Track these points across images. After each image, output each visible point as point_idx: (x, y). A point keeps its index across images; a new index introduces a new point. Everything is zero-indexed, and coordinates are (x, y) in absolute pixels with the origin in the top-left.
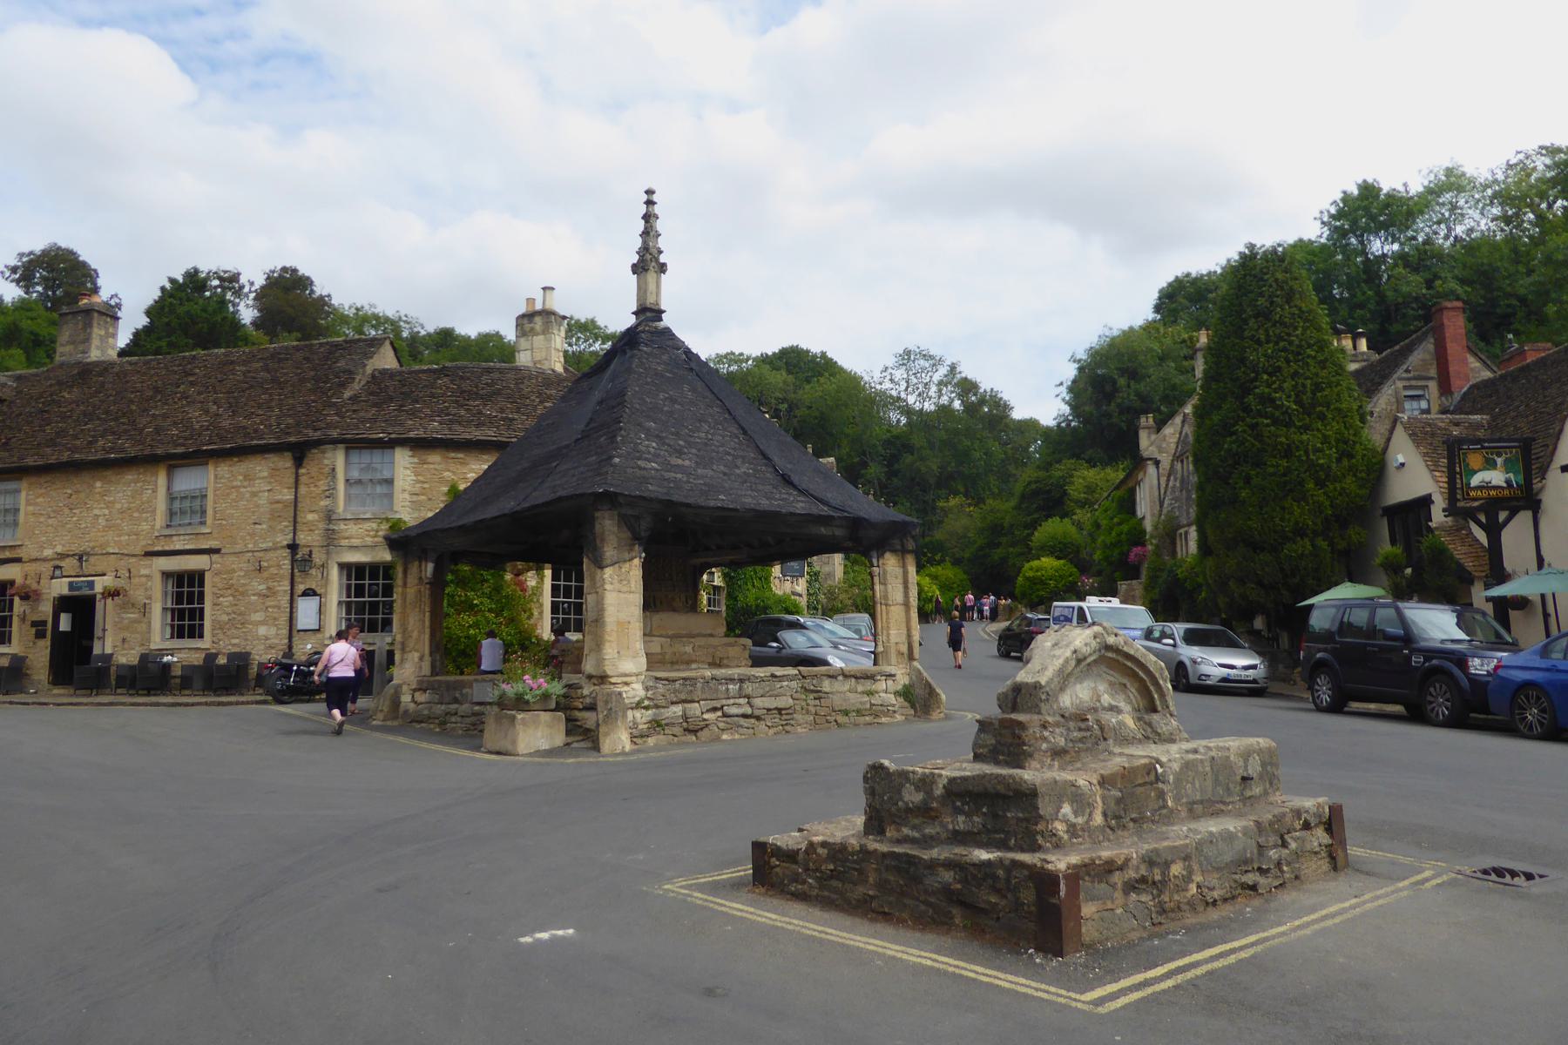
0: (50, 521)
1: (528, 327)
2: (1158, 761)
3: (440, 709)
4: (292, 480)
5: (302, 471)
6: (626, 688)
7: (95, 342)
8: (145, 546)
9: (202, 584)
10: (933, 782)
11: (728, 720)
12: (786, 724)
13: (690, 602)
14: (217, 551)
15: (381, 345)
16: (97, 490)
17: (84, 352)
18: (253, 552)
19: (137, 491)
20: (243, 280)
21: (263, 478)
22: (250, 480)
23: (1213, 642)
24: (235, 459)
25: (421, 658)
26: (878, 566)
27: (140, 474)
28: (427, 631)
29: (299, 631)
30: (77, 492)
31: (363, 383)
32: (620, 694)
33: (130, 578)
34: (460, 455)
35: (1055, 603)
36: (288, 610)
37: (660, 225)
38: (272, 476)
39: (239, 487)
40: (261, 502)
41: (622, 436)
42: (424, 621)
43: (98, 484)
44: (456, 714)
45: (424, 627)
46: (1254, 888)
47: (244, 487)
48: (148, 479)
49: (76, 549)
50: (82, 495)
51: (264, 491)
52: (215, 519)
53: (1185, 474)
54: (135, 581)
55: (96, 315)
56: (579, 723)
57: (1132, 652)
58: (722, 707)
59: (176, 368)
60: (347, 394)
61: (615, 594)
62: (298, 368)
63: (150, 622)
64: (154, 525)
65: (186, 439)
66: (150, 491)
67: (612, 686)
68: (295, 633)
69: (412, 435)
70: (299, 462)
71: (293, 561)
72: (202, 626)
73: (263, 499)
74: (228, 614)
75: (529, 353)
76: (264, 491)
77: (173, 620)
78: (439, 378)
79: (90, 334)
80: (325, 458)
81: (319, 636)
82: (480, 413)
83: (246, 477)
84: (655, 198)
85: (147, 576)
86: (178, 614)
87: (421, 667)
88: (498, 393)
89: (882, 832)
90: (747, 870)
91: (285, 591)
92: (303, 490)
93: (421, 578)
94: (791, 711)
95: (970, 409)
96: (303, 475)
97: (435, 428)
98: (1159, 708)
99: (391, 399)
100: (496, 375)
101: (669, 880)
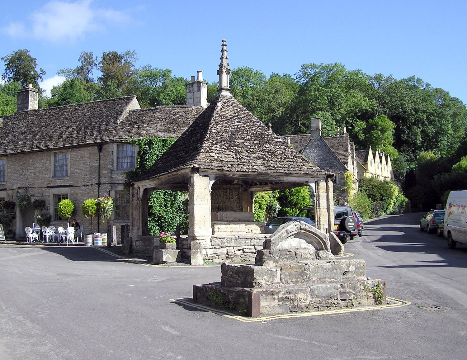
4: (98, 158)
7: (30, 103)
8: (47, 184)
11: (245, 254)
14: (72, 186)
16: (31, 163)
23: (376, 224)
24: (77, 150)
26: (316, 193)
35: (437, 205)
38: (90, 156)
47: (81, 161)
49: (24, 185)
50: (26, 165)
51: (88, 162)
58: (243, 249)
64: (50, 176)
66: (48, 163)
67: (197, 240)
76: (88, 162)
80: (110, 149)
88: (178, 118)
92: (102, 161)
93: (138, 198)
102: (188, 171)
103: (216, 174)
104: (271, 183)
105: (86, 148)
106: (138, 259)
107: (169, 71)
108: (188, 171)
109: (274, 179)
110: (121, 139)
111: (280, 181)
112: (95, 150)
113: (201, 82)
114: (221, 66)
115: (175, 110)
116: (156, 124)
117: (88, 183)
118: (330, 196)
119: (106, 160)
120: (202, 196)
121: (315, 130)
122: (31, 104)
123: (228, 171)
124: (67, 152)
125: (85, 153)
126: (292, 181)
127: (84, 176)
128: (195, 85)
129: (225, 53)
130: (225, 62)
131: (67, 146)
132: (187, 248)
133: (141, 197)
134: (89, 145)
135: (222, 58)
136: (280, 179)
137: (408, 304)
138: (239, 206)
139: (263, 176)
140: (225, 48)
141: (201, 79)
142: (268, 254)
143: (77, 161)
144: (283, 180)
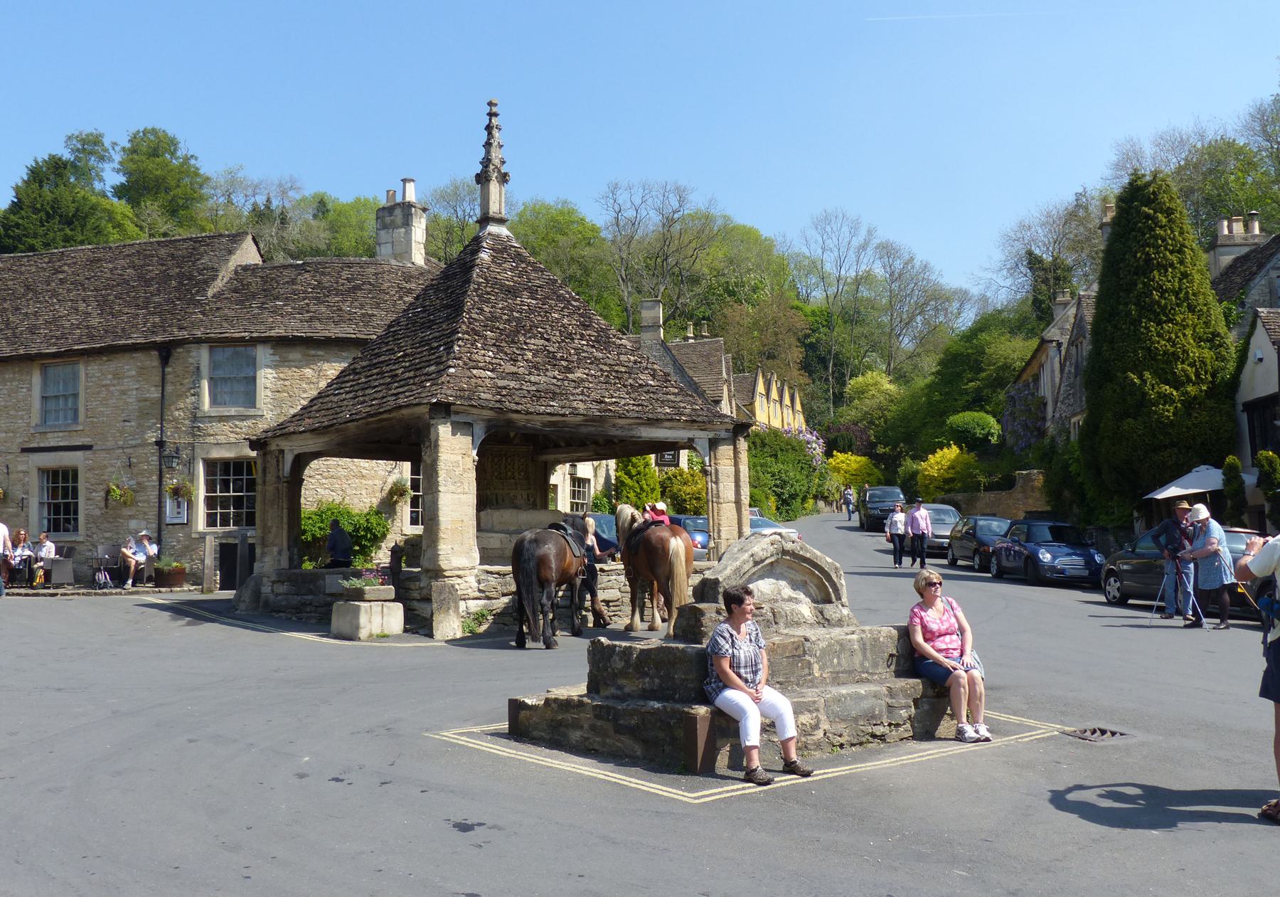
1: (388, 220)
2: (807, 640)
3: (296, 600)
4: (158, 379)
5: (168, 370)
6: (459, 581)
8: (21, 443)
9: (75, 479)
10: (631, 654)
12: (614, 615)
13: (532, 500)
15: (242, 241)
18: (123, 448)
19: (12, 389)
20: (107, 142)
21: (132, 376)
22: (119, 378)
24: (105, 359)
25: (280, 553)
26: (710, 466)
27: (14, 373)
28: (285, 527)
29: (167, 525)
31: (225, 280)
32: (453, 586)
33: (8, 473)
34: (320, 353)
36: (157, 505)
38: (139, 374)
39: (109, 385)
40: (130, 400)
41: (459, 346)
42: (282, 517)
44: (310, 604)
45: (282, 522)
46: (882, 738)
47: (114, 386)
48: (23, 378)
51: (132, 390)
52: (87, 417)
53: (1080, 360)
54: (13, 476)
56: (415, 612)
57: (808, 555)
59: (44, 265)
60: (210, 293)
61: (449, 496)
62: (163, 265)
63: (27, 516)
65: (57, 338)
66: (25, 390)
67: (446, 579)
68: (164, 527)
69: (273, 333)
71: (161, 457)
72: (76, 520)
73: (132, 399)
75: (389, 246)
76: (132, 390)
77: (49, 514)
78: (300, 274)
80: (191, 357)
81: (187, 529)
82: (340, 310)
85: (24, 472)
86: (55, 509)
87: (279, 561)
89: (597, 692)
90: (504, 726)
91: (154, 486)
92: (169, 388)
93: (278, 477)
94: (617, 603)
95: (894, 277)
96: (170, 373)
97: (295, 327)
98: (834, 600)
99: (254, 296)
100: (356, 269)
101: (448, 729)
102: (424, 410)
103: (489, 420)
104: (596, 443)
105: (127, 356)
108: (424, 410)
109: (619, 433)
110: (221, 333)
111: (632, 437)
112: (152, 360)
113: (413, 206)
114: (486, 162)
115: (351, 267)
116: (307, 301)
117: (131, 440)
118: (742, 475)
119: (181, 384)
120: (457, 473)
121: (649, 326)
123: (517, 412)
124: (77, 363)
126: (657, 438)
127: (122, 424)
128: (398, 212)
129: (495, 133)
130: (496, 155)
131: (76, 348)
132: (419, 598)
133: (286, 475)
134: (135, 348)
135: (488, 145)
136: (634, 433)
137: (1037, 734)
138: (528, 496)
139: (595, 426)
140: (494, 120)
141: (411, 196)
142: (714, 615)
143: (103, 386)
144: (639, 435)
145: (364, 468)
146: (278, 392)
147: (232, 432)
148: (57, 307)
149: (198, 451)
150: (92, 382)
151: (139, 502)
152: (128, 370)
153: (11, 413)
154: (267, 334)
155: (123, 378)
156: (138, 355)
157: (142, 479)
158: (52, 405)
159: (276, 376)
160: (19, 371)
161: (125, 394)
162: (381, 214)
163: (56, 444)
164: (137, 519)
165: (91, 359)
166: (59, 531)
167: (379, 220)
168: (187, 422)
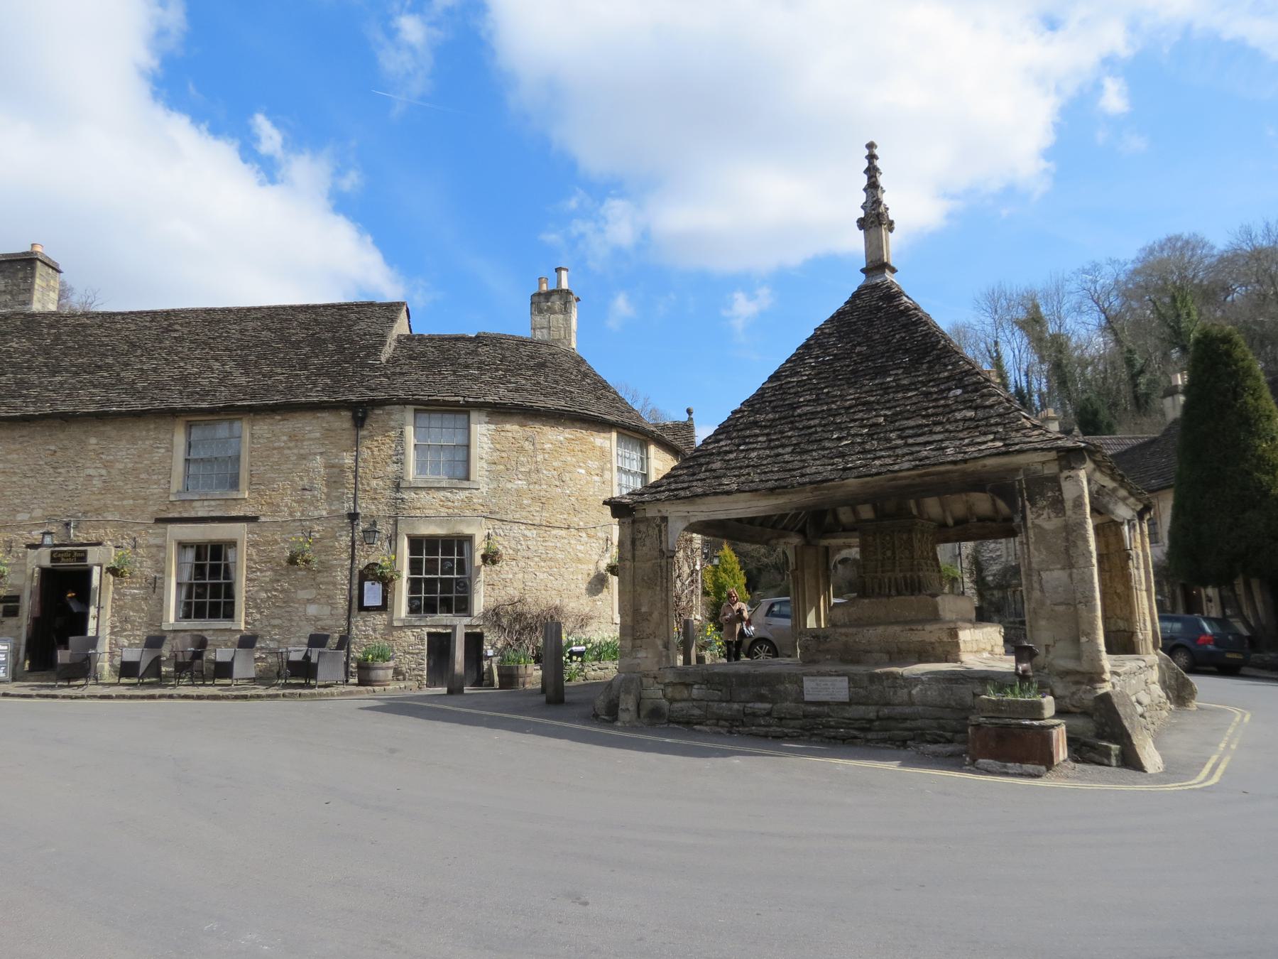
0: (26, 481)
5: (363, 433)
7: (37, 295)
16: (91, 447)
17: (25, 303)
27: (148, 430)
30: (65, 449)
37: (882, 180)
43: (93, 441)
50: (71, 453)
55: (39, 263)
66: (163, 451)
69: (489, 399)
70: (359, 422)
74: (266, 591)
79: (32, 284)
80: (392, 420)
83: (292, 438)
84: (876, 152)
85: (158, 546)
93: (661, 551)
106: (1218, 770)
107: (877, 158)
122: (38, 298)
125: (307, 428)
131: (239, 403)
143: (275, 449)
145: (580, 551)
146: (495, 463)
147: (443, 506)
148: (182, 364)
149: (401, 526)
150: (260, 443)
151: (321, 583)
152: (310, 432)
153: (142, 476)
154: (482, 400)
155: (303, 441)
156: (324, 415)
157: (327, 557)
158: (193, 469)
159: (492, 446)
160: (155, 428)
161: (304, 459)
162: (536, 299)
163: (205, 514)
164: (319, 604)
165: (258, 417)
166: (204, 617)
167: (534, 306)
168: (388, 493)
